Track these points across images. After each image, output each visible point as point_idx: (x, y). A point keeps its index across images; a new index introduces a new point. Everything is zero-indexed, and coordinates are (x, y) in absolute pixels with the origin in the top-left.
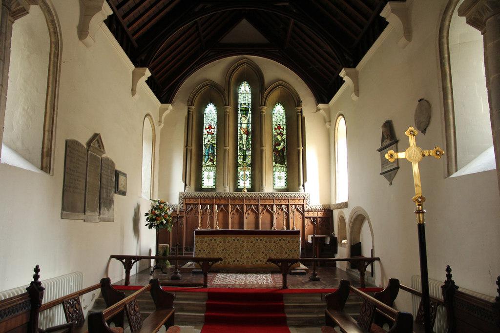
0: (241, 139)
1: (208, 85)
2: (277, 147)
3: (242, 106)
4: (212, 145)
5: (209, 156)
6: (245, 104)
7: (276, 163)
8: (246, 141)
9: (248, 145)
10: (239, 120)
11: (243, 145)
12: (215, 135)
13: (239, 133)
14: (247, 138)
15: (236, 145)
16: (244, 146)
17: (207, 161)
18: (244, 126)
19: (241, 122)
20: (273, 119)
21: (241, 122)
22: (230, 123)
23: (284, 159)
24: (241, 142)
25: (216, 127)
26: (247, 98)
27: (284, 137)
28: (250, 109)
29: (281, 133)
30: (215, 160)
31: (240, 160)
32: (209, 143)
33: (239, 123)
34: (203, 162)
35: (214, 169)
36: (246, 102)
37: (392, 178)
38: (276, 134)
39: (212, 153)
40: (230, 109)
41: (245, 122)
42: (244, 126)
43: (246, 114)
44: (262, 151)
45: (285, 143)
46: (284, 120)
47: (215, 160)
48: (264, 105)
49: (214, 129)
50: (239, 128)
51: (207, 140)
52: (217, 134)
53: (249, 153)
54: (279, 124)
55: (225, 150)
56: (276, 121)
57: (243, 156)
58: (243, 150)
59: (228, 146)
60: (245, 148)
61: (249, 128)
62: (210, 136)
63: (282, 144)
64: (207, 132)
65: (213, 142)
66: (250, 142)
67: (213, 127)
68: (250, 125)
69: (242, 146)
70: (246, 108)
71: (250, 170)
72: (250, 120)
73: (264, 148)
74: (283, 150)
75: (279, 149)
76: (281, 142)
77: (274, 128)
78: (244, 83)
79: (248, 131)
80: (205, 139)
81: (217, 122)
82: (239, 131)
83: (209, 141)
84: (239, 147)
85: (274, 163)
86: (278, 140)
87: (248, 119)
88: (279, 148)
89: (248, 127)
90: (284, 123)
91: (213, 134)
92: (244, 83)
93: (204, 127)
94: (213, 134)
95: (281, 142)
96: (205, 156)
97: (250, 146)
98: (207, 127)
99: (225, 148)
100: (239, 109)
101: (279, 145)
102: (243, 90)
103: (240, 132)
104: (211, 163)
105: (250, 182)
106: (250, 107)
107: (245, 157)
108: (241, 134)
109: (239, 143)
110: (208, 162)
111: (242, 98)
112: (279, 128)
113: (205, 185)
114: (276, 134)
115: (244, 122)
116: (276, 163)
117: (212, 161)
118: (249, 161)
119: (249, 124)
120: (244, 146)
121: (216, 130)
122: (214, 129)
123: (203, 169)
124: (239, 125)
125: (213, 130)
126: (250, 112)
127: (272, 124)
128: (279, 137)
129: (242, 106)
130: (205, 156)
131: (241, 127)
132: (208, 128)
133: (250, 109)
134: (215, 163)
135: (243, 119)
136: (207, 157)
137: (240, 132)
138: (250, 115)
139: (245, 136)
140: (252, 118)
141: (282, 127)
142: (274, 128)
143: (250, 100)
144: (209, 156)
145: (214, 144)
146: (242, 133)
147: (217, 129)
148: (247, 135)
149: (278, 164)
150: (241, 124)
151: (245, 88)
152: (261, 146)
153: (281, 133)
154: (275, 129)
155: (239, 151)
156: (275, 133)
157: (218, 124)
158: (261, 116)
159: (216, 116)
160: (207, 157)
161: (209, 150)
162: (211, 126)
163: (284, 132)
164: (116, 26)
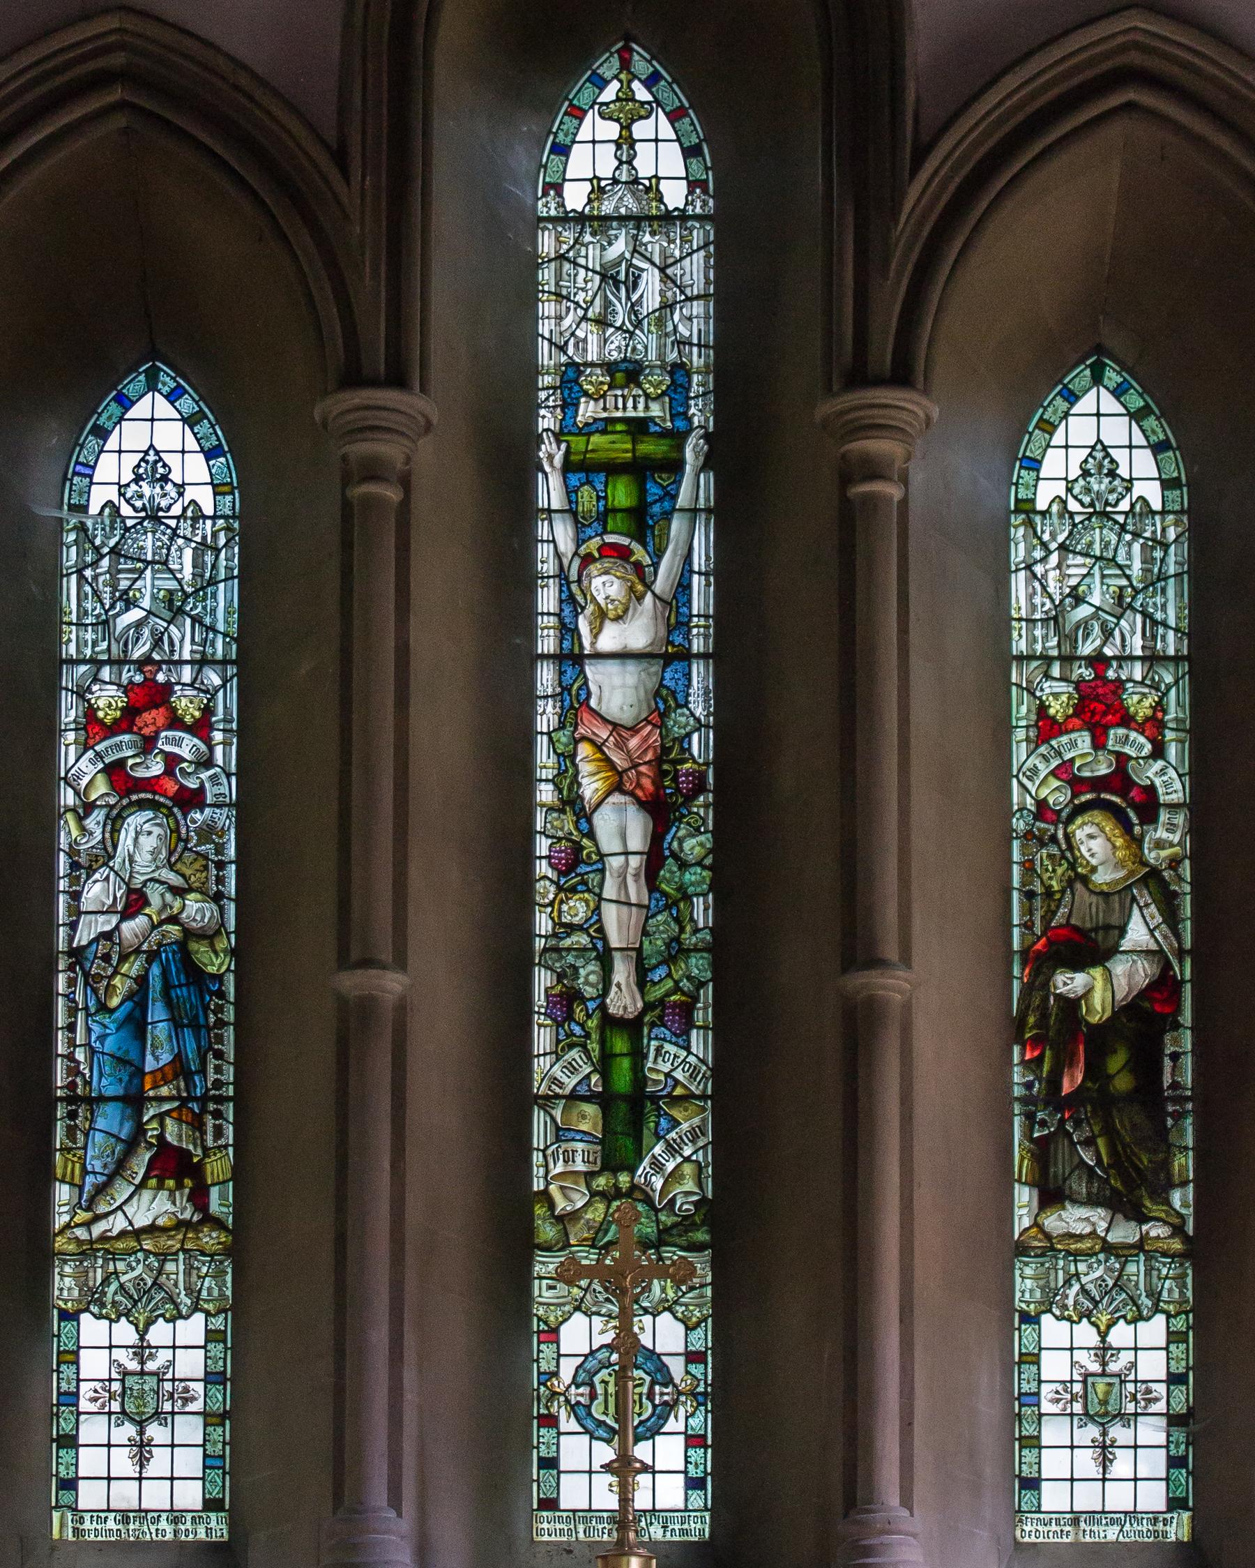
0: (578, 863)
1: (102, 80)
2: (1069, 983)
3: (587, 410)
4: (180, 961)
5: (134, 1101)
6: (627, 373)
7: (1051, 1197)
8: (636, 891)
9: (675, 952)
10: (548, 599)
11: (605, 959)
12: (224, 818)
13: (546, 794)
14: (655, 858)
15: (508, 958)
16: (622, 972)
17: (119, 1169)
18: (616, 691)
19: (567, 630)
20: (1019, 584)
21: (567, 630)
22: (419, 638)
23: (1162, 1142)
24: (577, 909)
25: (227, 704)
26: (651, 289)
27: (1167, 837)
28: (692, 452)
29: (1120, 779)
30: (218, 1167)
31: (560, 1166)
32: (133, 928)
33: (547, 643)
34: (63, 1193)
35: (217, 1284)
36: (648, 345)
37: (1127, 911)
38: (1057, 795)
39: (179, 1068)
40: (419, 435)
41: (617, 639)
42: (616, 691)
43: (643, 522)
44: (860, 1027)
45: (1171, 917)
46: (1171, 607)
47: (218, 1167)
48: (902, 376)
49: (202, 728)
50: (546, 716)
51: (95, 892)
52: (243, 808)
53: (679, 1061)
54: (1098, 661)
55: (354, 1022)
56: (1055, 619)
57: (605, 1100)
58: (609, 1022)
59: (401, 962)
60: (624, 999)
61: (679, 722)
62: (142, 838)
63: (1137, 933)
64: (115, 771)
65: (195, 909)
66: (702, 913)
67: (186, 704)
68: (700, 676)
69: (589, 973)
70: (638, 428)
71: (699, 1301)
72: (701, 597)
73: (892, 985)
74: (1144, 1017)
75: (1099, 1008)
76: (1119, 899)
77: (1022, 711)
78: (609, 66)
79: (668, 755)
80: (82, 868)
81: (244, 637)
82: (544, 758)
83: (135, 902)
84: (543, 980)
85: (1024, 1196)
86: (1079, 878)
87: (662, 583)
88: (1096, 990)
89: (663, 702)
90: (1170, 644)
91: (193, 799)
92: (609, 66)
93: (69, 711)
94: (193, 799)
95: (1119, 899)
96: (94, 1102)
97: (698, 965)
98: (108, 699)
99: (351, 982)
100: (551, 452)
101: (1090, 947)
102: (607, 166)
103: (567, 777)
104: (152, 1208)
105: (703, 1459)
106: (699, 413)
107: (629, 1115)
108: (571, 802)
109: (543, 923)
110: (122, 1191)
111: (585, 285)
112: (1099, 707)
113: (90, 1496)
114: (1057, 795)
115: (610, 639)
116: (1051, 1197)
117: (174, 1167)
118: (675, 1167)
119: (686, 656)
120: (622, 972)
121: (224, 754)
122: (202, 728)
123: (64, 1285)
124: (546, 677)
125: (187, 747)
126: (695, 486)
127: (1005, 659)
128: (1095, 842)
129: (587, 410)
130: (94, 1102)
131: (575, 704)
132: (127, 721)
133: (692, 452)
134: (213, 1092)
135: (606, 586)
136: (109, 1119)
137: (567, 777)
138: (692, 543)
139: (620, 828)
140: (722, 573)
141: (1139, 703)
142: (1022, 711)
143: (694, 321)
144: (134, 1101)
145: (209, 936)
146: (591, 787)
147: (245, 733)
148: (661, 812)
149: (1074, 1219)
150: (572, 658)
151: (626, 143)
152: (858, 951)
153: (1120, 779)
154: (1046, 728)
155: (543, 1039)
156: (1034, 779)
157: (255, 659)
158: (852, 527)
159: (228, 560)
160: (109, 1119)
161: (137, 1024)
162: (158, 695)
163: (1168, 779)
164: (675, 1002)
